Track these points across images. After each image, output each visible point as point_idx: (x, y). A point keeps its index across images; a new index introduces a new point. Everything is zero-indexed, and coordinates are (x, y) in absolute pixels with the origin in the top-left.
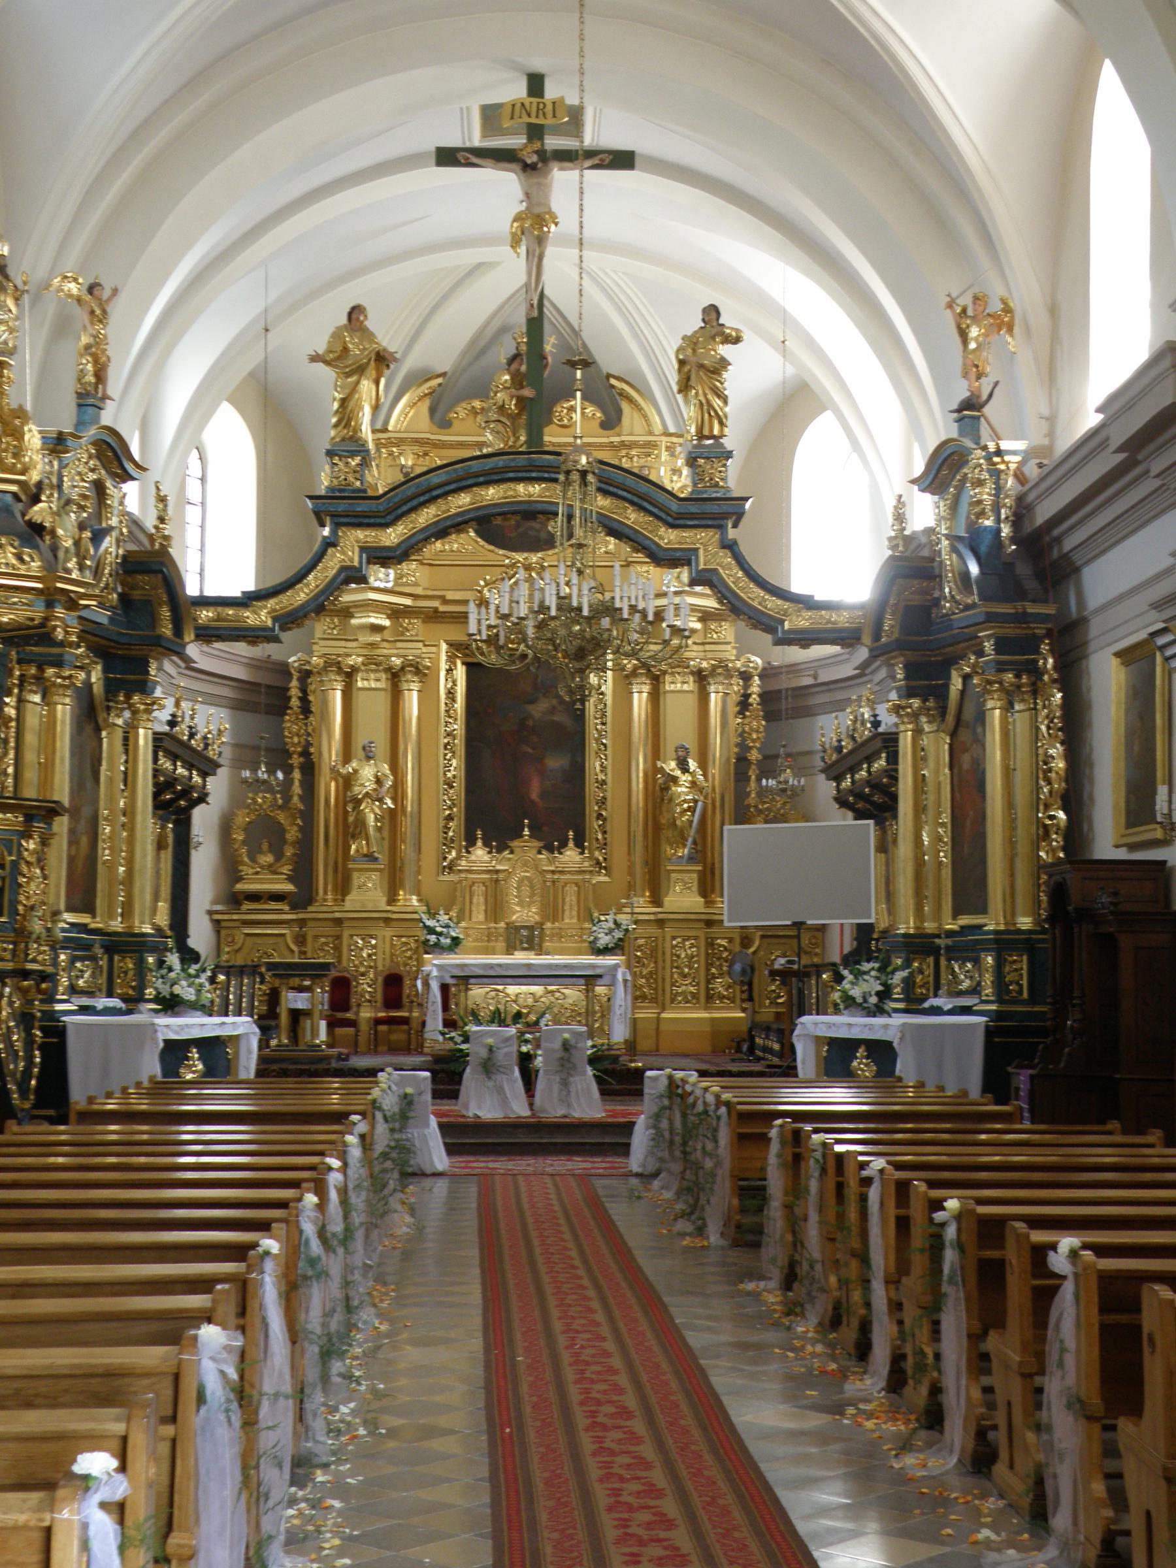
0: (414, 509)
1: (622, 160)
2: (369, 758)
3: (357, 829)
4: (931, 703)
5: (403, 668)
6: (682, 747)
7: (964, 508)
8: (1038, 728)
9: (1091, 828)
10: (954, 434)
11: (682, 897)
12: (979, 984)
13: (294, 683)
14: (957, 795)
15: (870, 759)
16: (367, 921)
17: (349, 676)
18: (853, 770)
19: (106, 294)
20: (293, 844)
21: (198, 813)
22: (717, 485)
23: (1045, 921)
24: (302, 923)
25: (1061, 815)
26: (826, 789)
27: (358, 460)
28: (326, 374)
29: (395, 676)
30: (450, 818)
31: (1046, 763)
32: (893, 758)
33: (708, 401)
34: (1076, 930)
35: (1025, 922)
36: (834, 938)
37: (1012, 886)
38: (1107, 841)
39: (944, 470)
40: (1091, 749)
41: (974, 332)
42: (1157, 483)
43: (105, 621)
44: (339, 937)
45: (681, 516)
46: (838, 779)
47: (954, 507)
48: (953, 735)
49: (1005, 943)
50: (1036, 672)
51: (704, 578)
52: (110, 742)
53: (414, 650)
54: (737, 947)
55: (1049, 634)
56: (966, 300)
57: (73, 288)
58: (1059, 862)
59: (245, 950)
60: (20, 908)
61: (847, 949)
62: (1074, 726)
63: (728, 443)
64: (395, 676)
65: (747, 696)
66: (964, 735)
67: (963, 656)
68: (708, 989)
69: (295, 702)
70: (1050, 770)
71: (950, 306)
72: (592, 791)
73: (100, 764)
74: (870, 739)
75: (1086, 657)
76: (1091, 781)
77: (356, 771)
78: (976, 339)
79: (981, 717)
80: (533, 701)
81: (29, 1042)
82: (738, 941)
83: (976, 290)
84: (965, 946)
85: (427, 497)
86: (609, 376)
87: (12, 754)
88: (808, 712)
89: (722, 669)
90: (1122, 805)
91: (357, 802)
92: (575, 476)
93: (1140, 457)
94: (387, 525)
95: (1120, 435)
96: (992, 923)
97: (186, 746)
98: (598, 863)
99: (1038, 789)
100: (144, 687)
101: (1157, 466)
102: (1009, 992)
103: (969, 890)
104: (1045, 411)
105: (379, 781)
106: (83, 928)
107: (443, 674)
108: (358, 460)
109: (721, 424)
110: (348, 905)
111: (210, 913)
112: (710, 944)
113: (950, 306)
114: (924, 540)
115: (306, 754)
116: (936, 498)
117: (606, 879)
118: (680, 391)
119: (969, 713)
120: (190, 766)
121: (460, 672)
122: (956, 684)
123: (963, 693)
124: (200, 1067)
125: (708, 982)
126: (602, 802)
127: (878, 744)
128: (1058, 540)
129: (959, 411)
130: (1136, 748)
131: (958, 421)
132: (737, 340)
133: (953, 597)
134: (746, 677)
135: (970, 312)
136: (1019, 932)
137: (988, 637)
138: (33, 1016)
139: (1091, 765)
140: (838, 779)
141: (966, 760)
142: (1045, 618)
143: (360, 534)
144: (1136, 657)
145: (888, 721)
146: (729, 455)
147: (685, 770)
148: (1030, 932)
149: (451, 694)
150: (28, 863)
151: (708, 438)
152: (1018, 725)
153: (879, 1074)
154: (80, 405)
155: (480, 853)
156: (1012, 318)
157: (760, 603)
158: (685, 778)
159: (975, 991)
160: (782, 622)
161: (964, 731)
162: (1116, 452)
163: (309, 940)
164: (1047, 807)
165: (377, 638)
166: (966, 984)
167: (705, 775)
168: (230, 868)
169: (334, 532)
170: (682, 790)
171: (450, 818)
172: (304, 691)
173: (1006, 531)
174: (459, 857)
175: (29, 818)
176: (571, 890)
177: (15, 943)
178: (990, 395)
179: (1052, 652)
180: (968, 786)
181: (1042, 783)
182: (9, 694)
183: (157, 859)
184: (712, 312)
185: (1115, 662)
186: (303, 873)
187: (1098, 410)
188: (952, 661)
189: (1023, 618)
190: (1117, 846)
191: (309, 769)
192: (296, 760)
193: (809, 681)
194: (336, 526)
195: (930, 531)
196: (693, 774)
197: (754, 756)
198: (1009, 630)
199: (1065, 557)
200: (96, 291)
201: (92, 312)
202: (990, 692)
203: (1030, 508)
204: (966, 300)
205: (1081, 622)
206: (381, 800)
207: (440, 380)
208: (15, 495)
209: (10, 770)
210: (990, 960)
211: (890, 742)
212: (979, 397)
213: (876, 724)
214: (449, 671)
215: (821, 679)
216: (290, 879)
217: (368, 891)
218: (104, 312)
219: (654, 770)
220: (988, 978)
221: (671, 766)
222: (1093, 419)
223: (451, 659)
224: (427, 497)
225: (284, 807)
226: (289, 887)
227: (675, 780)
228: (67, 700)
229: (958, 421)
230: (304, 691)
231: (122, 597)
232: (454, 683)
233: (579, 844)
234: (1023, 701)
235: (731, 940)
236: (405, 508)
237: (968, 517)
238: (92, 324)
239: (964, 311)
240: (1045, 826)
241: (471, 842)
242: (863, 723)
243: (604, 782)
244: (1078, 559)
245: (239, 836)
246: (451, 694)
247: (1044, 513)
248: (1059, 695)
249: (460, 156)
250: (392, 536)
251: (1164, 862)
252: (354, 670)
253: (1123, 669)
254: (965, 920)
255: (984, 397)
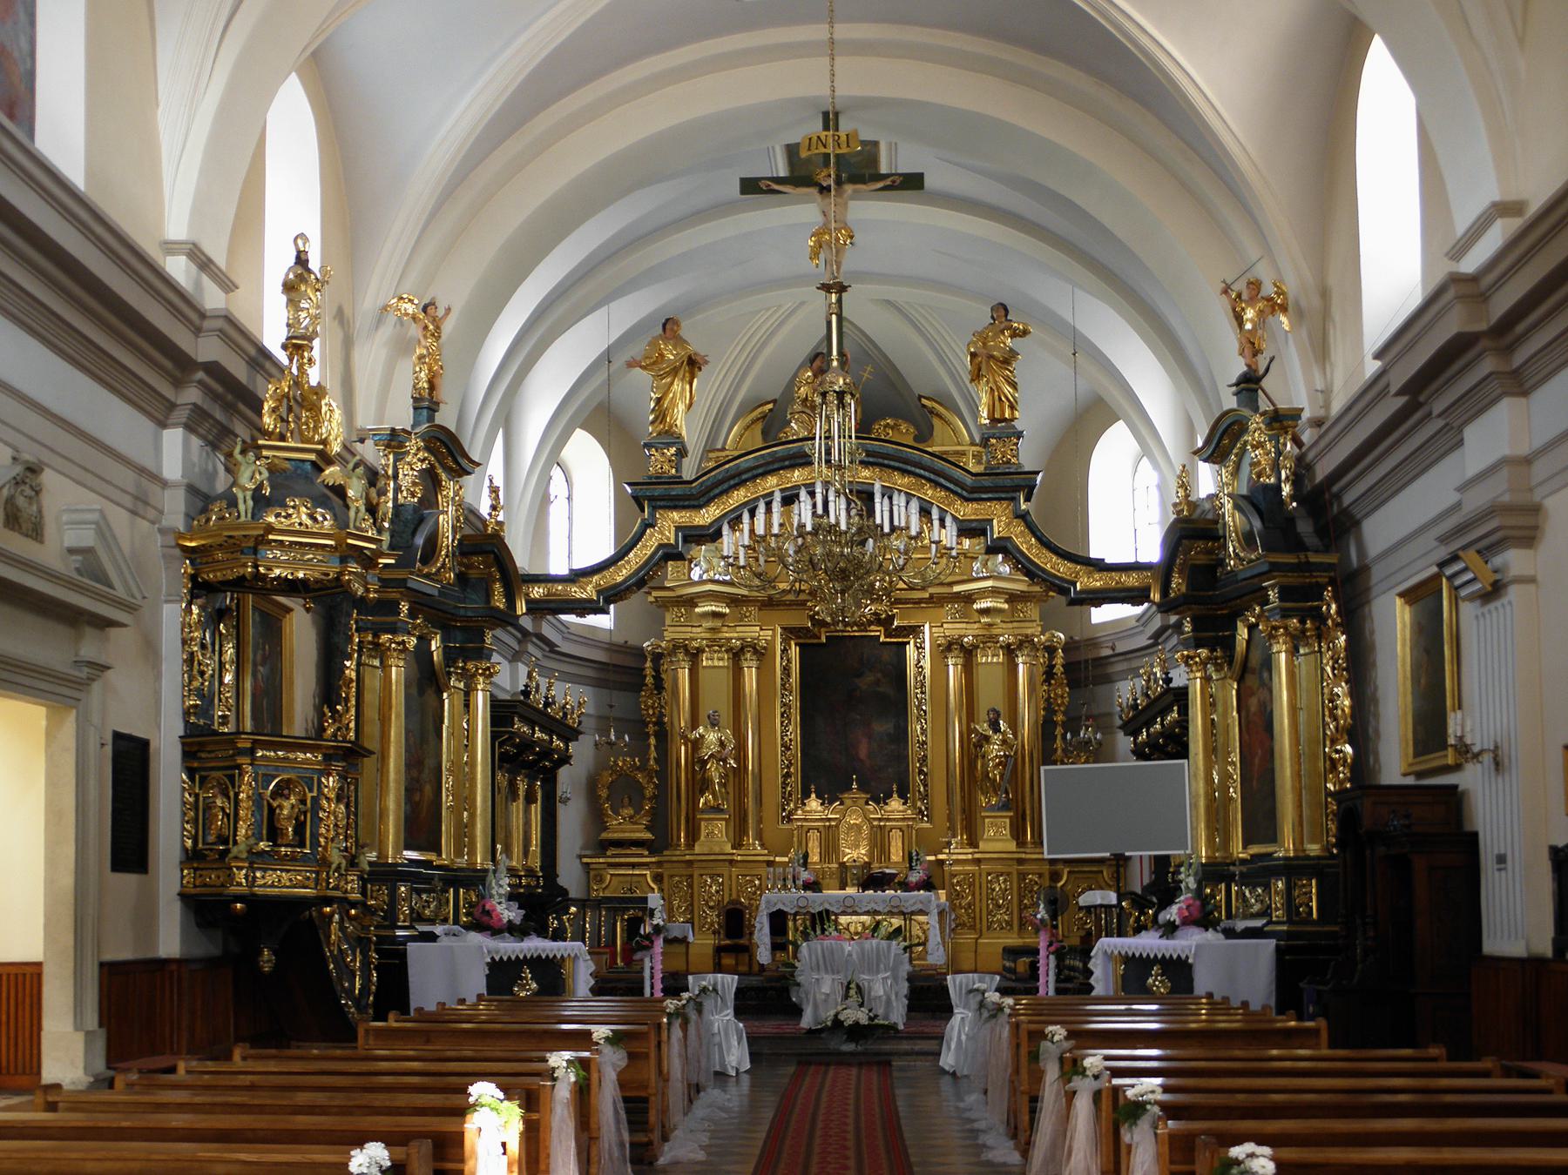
0: (726, 492)
1: (912, 182)
2: (713, 725)
3: (704, 785)
4: (1219, 653)
5: (742, 648)
6: (994, 710)
7: (1245, 469)
8: (1323, 670)
9: (1377, 760)
10: (1235, 406)
11: (997, 837)
12: (1269, 907)
13: (648, 664)
14: (1246, 737)
15: (1164, 712)
16: (715, 863)
17: (695, 656)
18: (1149, 723)
19: (441, 312)
20: (650, 799)
21: (563, 773)
22: (1009, 461)
23: (1334, 846)
24: (659, 864)
25: (1348, 749)
26: (1125, 743)
27: (673, 450)
28: (642, 377)
29: (737, 655)
30: (788, 775)
31: (1331, 701)
32: (1184, 711)
33: (999, 388)
34: (1368, 852)
35: (1314, 849)
36: (1135, 868)
37: (1301, 816)
38: (1395, 764)
39: (1221, 443)
40: (1376, 688)
41: (1250, 314)
42: (1440, 423)
43: (436, 593)
44: (691, 876)
45: (973, 490)
46: (1135, 733)
47: (1236, 472)
48: (1240, 681)
49: (1294, 869)
50: (1320, 618)
51: (1000, 547)
52: (449, 703)
53: (751, 632)
54: (1047, 883)
55: (1332, 582)
56: (1240, 286)
57: (410, 309)
58: (1343, 791)
59: (611, 888)
60: (322, 840)
61: (1146, 881)
62: (1358, 667)
63: (1018, 425)
64: (737, 655)
65: (1051, 667)
66: (1251, 680)
67: (1250, 608)
68: (1021, 918)
69: (649, 680)
70: (1336, 708)
71: (1225, 292)
72: (913, 750)
73: (442, 722)
74: (1162, 694)
75: (1368, 602)
76: (1377, 716)
77: (702, 737)
78: (1251, 320)
79: (1268, 663)
80: (859, 675)
81: (366, 963)
82: (1047, 876)
83: (1250, 276)
84: (1260, 872)
85: (737, 480)
86: (920, 397)
87: (353, 711)
88: (1108, 680)
89: (1025, 642)
90: (1410, 735)
91: (704, 763)
92: (831, 397)
93: (1422, 399)
94: (700, 507)
95: (1398, 379)
96: (1286, 847)
97: (544, 713)
98: (921, 812)
99: (1325, 725)
100: (481, 654)
101: (1438, 406)
102: (1298, 913)
103: (1261, 823)
104: (1319, 385)
105: (722, 744)
106: (427, 864)
107: (778, 653)
108: (673, 450)
109: (1012, 407)
110: (697, 849)
111: (580, 857)
112: (1022, 876)
113: (1225, 292)
114: (1207, 506)
115: (659, 723)
116: (1217, 467)
117: (928, 825)
118: (972, 380)
119: (1255, 660)
120: (550, 733)
121: (794, 651)
122: (1243, 633)
123: (1249, 642)
124: (534, 985)
125: (1021, 911)
126: (924, 760)
127: (1170, 698)
128: (1338, 497)
129: (1237, 384)
130: (1423, 681)
131: (1236, 394)
132: (1025, 333)
133: (1237, 555)
134: (1051, 650)
135: (1245, 297)
136: (1308, 858)
137: (1273, 587)
138: (369, 940)
139: (1376, 701)
140: (1135, 733)
141: (1253, 703)
142: (1330, 567)
143: (675, 515)
144: (1423, 596)
145: (1179, 677)
146: (1019, 435)
147: (997, 730)
148: (1318, 858)
149: (786, 670)
150: (328, 799)
151: (1000, 421)
152: (1303, 667)
153: (1172, 991)
154: (415, 409)
155: (814, 804)
156: (1286, 298)
157: (1059, 574)
158: (997, 738)
159: (1265, 912)
160: (1074, 584)
161: (1252, 675)
162: (1399, 394)
163: (666, 879)
164: (1333, 742)
165: (718, 623)
166: (1257, 908)
167: (1015, 735)
168: (597, 817)
169: (652, 515)
170: (994, 749)
171: (788, 775)
172: (657, 670)
173: (1286, 489)
174: (796, 809)
175: (328, 758)
176: (896, 834)
177: (317, 873)
178: (1267, 370)
179: (1336, 598)
180: (1258, 726)
181: (1328, 719)
182: (350, 658)
183: (527, 811)
184: (1002, 310)
185: (1399, 602)
186: (660, 823)
187: (1377, 356)
188: (1237, 614)
189: (1306, 567)
190: (1405, 775)
191: (663, 735)
192: (651, 729)
193: (1108, 652)
194: (654, 508)
195: (1211, 497)
196: (1004, 733)
197: (1060, 718)
198: (1292, 579)
199: (1345, 512)
200: (430, 310)
201: (426, 327)
202: (1275, 637)
203: (1310, 468)
204: (1240, 286)
205: (1364, 569)
206: (725, 761)
207: (770, 406)
208: (313, 463)
209: (352, 725)
210: (1280, 884)
211: (1181, 696)
212: (1256, 371)
213: (1168, 680)
214: (784, 651)
215: (1119, 649)
216: (648, 828)
217: (716, 835)
218: (438, 328)
219: (967, 732)
220: (1278, 901)
221: (983, 728)
222: (1372, 367)
223: (786, 641)
224: (737, 480)
225: (643, 768)
226: (648, 836)
227: (987, 739)
228: (401, 663)
229: (1236, 394)
230: (657, 670)
231: (458, 576)
232: (789, 661)
233: (903, 796)
234: (1307, 645)
235: (1040, 875)
236: (717, 491)
237: (1250, 478)
238: (425, 337)
239: (1239, 296)
240: (1332, 759)
241: (806, 795)
242: (1156, 681)
243: (924, 743)
244: (1357, 512)
245: (604, 793)
246: (786, 670)
247: (1322, 470)
248: (1343, 638)
249: (762, 185)
250: (706, 516)
251: (1456, 787)
252: (700, 651)
253: (1407, 608)
254: (1255, 849)
255: (1261, 371)
